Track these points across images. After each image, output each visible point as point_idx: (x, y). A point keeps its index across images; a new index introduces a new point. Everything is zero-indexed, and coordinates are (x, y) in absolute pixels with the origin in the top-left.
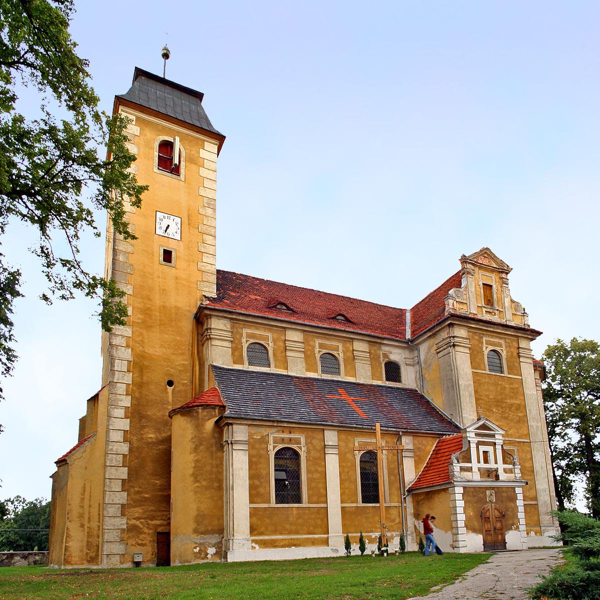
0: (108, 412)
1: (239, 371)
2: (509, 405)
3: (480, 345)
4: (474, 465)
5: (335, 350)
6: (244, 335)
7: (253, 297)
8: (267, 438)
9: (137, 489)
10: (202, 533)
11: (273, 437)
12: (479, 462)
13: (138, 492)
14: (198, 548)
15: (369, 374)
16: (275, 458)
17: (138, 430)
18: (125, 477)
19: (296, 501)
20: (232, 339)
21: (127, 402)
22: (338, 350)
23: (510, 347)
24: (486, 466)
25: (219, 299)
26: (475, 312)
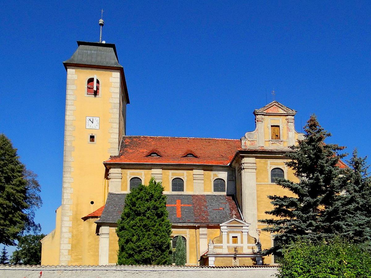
4: (225, 244)
5: (182, 176)
6: (129, 174)
12: (228, 242)
13: (76, 255)
15: (202, 189)
21: (70, 213)
22: (183, 175)
24: (235, 245)
26: (262, 145)
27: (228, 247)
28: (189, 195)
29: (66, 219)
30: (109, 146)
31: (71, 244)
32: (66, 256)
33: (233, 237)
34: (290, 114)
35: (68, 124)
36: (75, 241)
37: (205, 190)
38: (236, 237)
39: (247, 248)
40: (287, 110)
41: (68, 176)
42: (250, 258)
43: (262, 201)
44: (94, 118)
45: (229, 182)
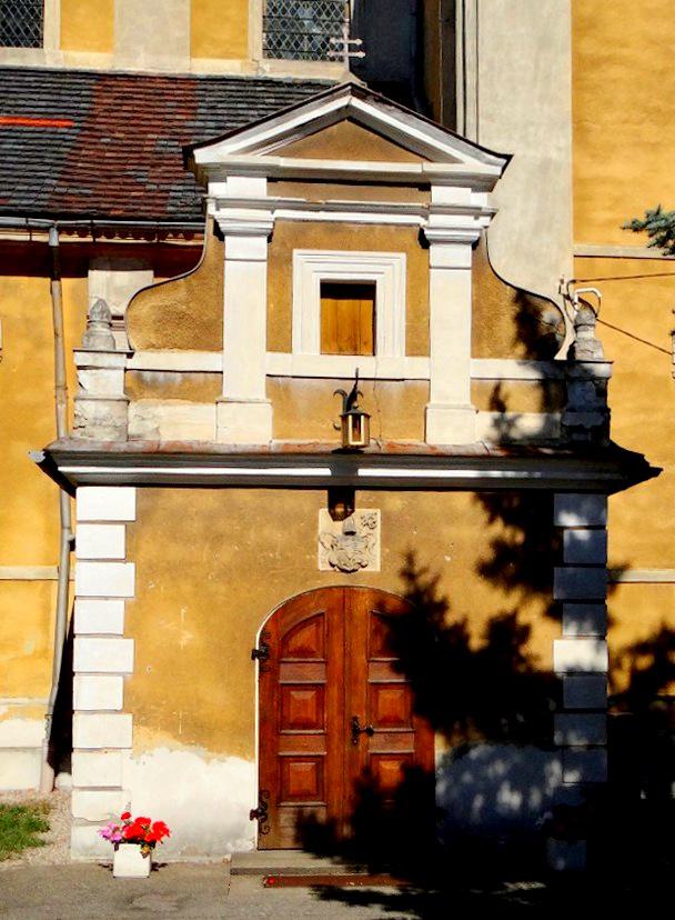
4: (243, 355)
12: (279, 337)
15: (180, 32)
24: (344, 366)
27: (278, 385)
28: (75, 74)
33: (330, 290)
37: (196, 46)
38: (366, 291)
39: (467, 401)
42: (463, 499)
43: (609, 60)
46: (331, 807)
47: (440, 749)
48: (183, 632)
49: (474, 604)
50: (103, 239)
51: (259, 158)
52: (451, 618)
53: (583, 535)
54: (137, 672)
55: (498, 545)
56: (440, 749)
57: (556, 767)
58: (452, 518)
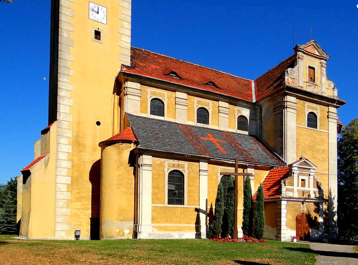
0: (57, 140)
1: (144, 118)
2: (317, 149)
3: (303, 108)
4: (295, 188)
6: (149, 93)
7: (154, 67)
8: (164, 163)
9: (77, 191)
10: (121, 221)
11: (168, 163)
12: (298, 186)
13: (78, 193)
14: (118, 230)
15: (227, 125)
16: (168, 176)
17: (77, 153)
18: (69, 182)
19: (180, 203)
20: (141, 95)
22: (209, 106)
23: (323, 111)
24: (303, 188)
25: (133, 67)
26: (301, 85)
29: (63, 141)
30: (118, 50)
31: (71, 177)
32: (65, 193)
34: (324, 58)
35: (64, 5)
36: (76, 173)
40: (322, 53)
41: (65, 80)
44: (100, 7)
45: (252, 121)
46: (303, 236)
47: (310, 230)
48: (290, 217)
49: (313, 215)
50: (250, 165)
51: (296, 166)
52: (311, 216)
53: (322, 208)
54: (287, 221)
55: (315, 208)
56: (310, 230)
57: (319, 232)
58: (311, 205)
